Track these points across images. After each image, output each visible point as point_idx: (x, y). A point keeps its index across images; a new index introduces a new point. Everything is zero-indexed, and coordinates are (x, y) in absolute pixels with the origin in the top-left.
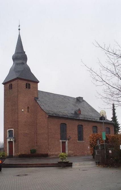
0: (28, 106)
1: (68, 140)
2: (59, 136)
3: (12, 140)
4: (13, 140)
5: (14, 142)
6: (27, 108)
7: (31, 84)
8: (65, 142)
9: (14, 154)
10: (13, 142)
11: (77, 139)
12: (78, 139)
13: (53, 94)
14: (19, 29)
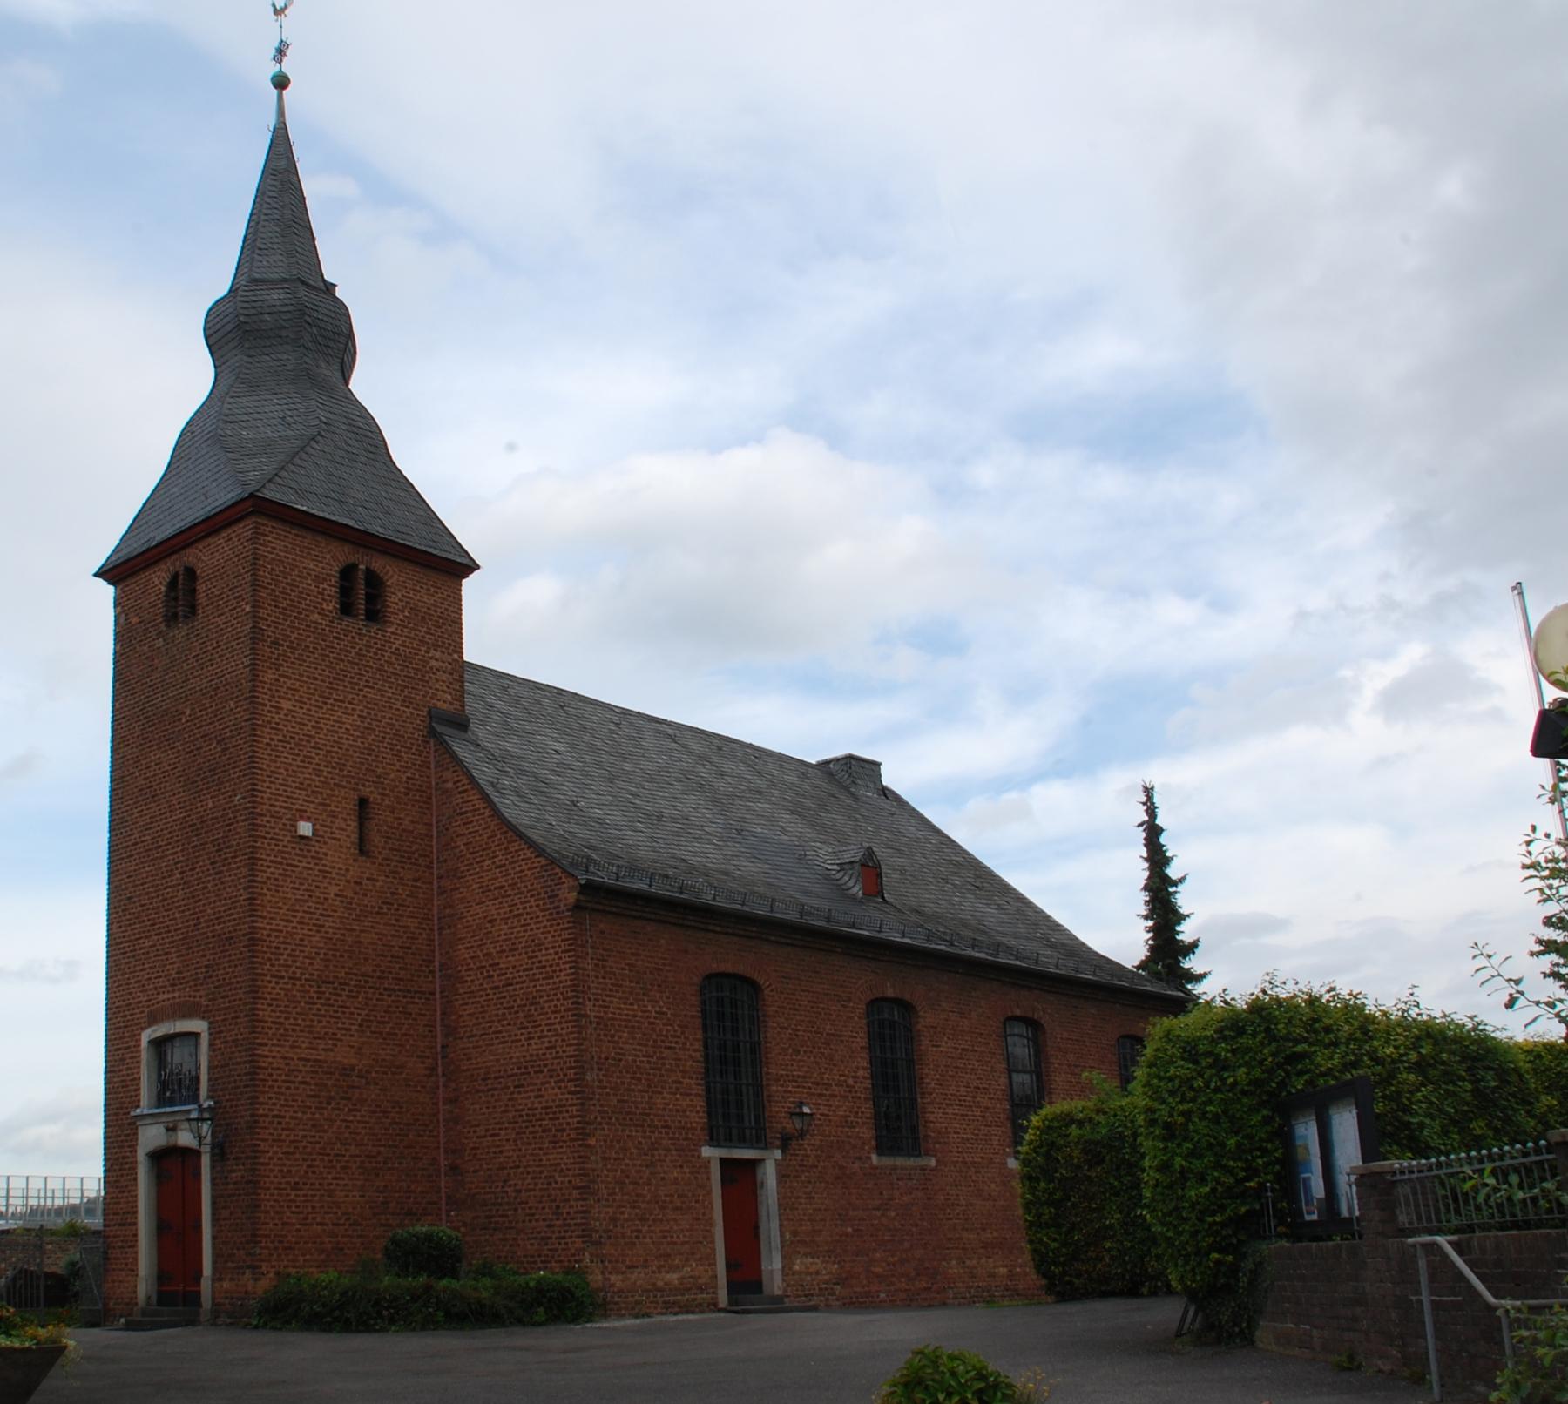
0: (366, 791)
1: (784, 1148)
2: (695, 1110)
3: (185, 1138)
4: (200, 1138)
5: (206, 1161)
6: (351, 806)
7: (395, 576)
8: (753, 1164)
9: (206, 1286)
10: (197, 1154)
11: (867, 1133)
12: (878, 1138)
13: (609, 707)
14: (281, 83)
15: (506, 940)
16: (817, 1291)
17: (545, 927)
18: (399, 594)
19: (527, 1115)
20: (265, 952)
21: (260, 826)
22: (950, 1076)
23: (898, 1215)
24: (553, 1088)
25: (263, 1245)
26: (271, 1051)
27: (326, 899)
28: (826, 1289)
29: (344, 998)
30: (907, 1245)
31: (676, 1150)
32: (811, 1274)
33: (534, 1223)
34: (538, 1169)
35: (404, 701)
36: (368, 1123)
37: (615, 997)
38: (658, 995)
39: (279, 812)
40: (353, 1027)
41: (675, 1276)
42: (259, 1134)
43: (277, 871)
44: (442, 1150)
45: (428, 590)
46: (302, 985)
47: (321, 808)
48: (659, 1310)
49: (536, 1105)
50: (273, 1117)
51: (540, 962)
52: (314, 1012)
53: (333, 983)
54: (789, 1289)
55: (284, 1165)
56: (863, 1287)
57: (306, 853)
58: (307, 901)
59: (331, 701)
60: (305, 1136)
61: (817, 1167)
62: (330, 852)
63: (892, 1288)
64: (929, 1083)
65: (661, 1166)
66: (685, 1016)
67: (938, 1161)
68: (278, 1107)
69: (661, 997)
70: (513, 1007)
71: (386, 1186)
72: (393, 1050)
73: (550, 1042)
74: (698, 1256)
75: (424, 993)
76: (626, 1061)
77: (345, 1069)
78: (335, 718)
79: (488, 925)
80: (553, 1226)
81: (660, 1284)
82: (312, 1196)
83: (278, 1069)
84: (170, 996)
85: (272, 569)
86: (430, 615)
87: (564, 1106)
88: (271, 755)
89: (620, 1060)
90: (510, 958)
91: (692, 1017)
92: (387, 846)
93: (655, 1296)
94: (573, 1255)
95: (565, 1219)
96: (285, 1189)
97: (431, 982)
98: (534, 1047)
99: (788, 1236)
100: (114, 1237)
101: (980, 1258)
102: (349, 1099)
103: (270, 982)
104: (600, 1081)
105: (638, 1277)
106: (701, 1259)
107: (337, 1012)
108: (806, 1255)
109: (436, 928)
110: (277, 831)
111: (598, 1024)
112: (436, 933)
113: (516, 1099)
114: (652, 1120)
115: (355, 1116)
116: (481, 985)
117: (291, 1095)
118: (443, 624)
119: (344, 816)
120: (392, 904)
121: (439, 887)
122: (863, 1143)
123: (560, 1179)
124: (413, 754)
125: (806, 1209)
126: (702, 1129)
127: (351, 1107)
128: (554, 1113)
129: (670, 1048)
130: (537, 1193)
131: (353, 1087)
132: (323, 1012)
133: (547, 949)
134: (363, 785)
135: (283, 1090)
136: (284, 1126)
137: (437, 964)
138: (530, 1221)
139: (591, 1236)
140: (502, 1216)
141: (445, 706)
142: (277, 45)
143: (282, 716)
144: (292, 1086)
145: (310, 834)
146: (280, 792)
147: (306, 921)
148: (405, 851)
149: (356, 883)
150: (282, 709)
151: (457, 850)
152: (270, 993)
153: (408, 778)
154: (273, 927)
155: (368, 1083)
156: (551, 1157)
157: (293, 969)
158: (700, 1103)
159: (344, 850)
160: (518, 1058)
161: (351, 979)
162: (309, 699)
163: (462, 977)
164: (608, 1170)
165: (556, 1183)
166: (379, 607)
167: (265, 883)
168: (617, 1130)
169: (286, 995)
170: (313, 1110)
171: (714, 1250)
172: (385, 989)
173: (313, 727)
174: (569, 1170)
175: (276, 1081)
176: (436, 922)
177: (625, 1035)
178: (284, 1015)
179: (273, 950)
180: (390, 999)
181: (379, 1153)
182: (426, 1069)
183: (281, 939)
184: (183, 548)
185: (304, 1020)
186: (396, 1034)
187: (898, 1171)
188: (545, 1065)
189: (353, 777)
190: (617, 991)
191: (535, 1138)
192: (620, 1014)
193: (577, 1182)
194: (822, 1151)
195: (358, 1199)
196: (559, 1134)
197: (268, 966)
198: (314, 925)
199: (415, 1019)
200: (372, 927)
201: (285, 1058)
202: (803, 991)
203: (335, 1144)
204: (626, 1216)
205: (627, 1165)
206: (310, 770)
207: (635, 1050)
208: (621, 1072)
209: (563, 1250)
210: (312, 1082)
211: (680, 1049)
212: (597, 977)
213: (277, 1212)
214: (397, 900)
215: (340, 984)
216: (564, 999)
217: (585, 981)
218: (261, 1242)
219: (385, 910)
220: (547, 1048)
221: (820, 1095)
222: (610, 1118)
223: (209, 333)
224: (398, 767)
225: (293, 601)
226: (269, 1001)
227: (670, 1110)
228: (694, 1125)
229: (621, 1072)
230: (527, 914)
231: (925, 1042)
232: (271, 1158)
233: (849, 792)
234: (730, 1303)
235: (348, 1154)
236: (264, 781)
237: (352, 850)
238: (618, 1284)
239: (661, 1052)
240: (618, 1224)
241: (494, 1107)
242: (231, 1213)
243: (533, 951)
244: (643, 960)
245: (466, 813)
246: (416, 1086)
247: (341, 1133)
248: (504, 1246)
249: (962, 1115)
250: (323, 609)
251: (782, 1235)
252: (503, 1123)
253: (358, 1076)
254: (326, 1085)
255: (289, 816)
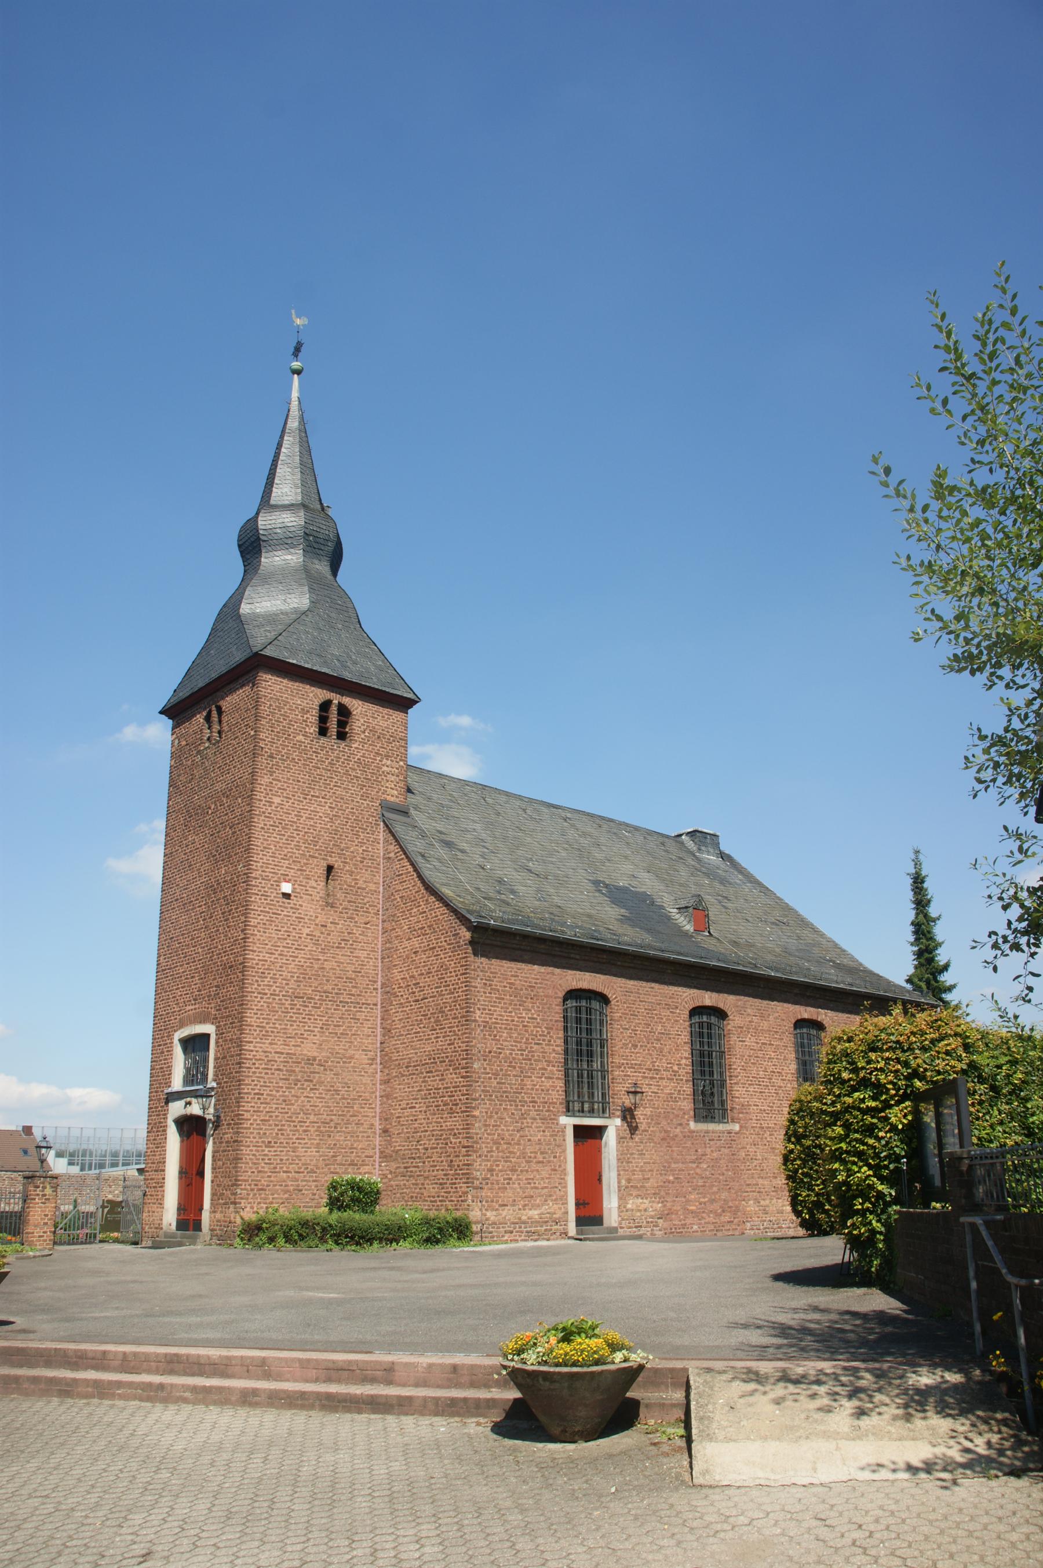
0: (331, 861)
2: (555, 1087)
6: (322, 871)
9: (206, 1217)
11: (687, 1105)
15: (424, 966)
16: (645, 1223)
17: (450, 957)
18: (362, 721)
19: (434, 1093)
20: (254, 976)
21: (254, 886)
22: (752, 1063)
23: (708, 1167)
24: (451, 1074)
25: (243, 1187)
26: (255, 1047)
27: (300, 938)
28: (652, 1222)
29: (310, 1008)
30: (715, 1189)
31: (541, 1119)
32: (640, 1211)
33: (435, 1172)
34: (440, 1133)
35: (362, 796)
36: (324, 1098)
37: (498, 1007)
38: (530, 1005)
39: (268, 876)
40: (316, 1029)
41: (536, 1212)
42: (244, 1106)
43: (265, 918)
44: (378, 1118)
45: (383, 717)
46: (279, 1000)
47: (299, 873)
48: (523, 1238)
49: (440, 1086)
50: (255, 1094)
51: (446, 982)
52: (288, 1018)
53: (302, 998)
54: (623, 1222)
55: (261, 1129)
56: (680, 1221)
57: (286, 905)
58: (286, 939)
59: (310, 797)
60: (277, 1108)
61: (647, 1131)
62: (304, 904)
63: (703, 1222)
64: (736, 1069)
65: (529, 1131)
66: (551, 1020)
67: (741, 1127)
68: (258, 1087)
69: (533, 1007)
70: (427, 1015)
71: (335, 1145)
72: (345, 1045)
73: (450, 1040)
74: (554, 1198)
75: (369, 1004)
76: (505, 1053)
77: (309, 1060)
78: (312, 809)
79: (413, 955)
80: (448, 1174)
81: (524, 1218)
82: (281, 1151)
83: (260, 1060)
84: (193, 1007)
85: (271, 705)
86: (383, 734)
87: (458, 1087)
88: (264, 836)
89: (500, 1053)
90: (427, 979)
91: (556, 1021)
92: (346, 899)
93: (520, 1227)
94: (461, 1197)
95: (456, 1170)
96: (261, 1147)
97: (375, 996)
98: (441, 1043)
99: (623, 1182)
100: (151, 1179)
101: (772, 1199)
102: (311, 1081)
103: (256, 997)
104: (485, 1069)
105: (507, 1213)
106: (556, 1200)
107: (304, 1018)
108: (637, 1196)
109: (380, 957)
110: (266, 889)
111: (485, 1027)
112: (380, 961)
113: (427, 1081)
114: (523, 1097)
115: (315, 1094)
116: (407, 998)
117: (269, 1078)
118: (394, 741)
119: (316, 878)
120: (348, 941)
121: (383, 928)
122: (684, 1113)
123: (453, 1141)
124: (368, 833)
125: (639, 1163)
126: (561, 1103)
127: (312, 1087)
128: (452, 1092)
129: (538, 1044)
130: (438, 1150)
131: (314, 1073)
132: (294, 1019)
133: (451, 972)
134: (331, 856)
135: (263, 1075)
136: (262, 1101)
137: (379, 983)
138: (433, 1171)
139: (473, 1183)
140: (415, 1167)
141: (392, 799)
142: (300, 354)
143: (273, 808)
144: (269, 1071)
145: (290, 892)
146: (270, 862)
147: (285, 953)
148: (360, 903)
149: (322, 926)
150: (273, 803)
151: (395, 902)
152: (256, 1005)
153: (363, 850)
154: (260, 958)
155: (325, 1070)
156: (448, 1124)
157: (274, 988)
158: (560, 1084)
159: (315, 903)
160: (429, 1051)
161: (316, 995)
162: (294, 796)
163: (395, 993)
164: (488, 1134)
165: (451, 1143)
166: (347, 730)
167: (256, 927)
168: (496, 1105)
169: (268, 1007)
170: (284, 1090)
171: (566, 1193)
172: (341, 1002)
173: (296, 815)
174: (459, 1133)
175: (258, 1068)
176: (380, 953)
177: (505, 1035)
178: (265, 1021)
179: (260, 974)
180: (344, 1009)
181: (332, 1120)
182: (369, 1059)
183: (266, 967)
184: (215, 692)
185: (280, 1024)
186: (347, 1034)
187: (710, 1134)
188: (447, 1057)
189: (323, 851)
190: (500, 1003)
191: (438, 1110)
192: (501, 1020)
193: (465, 1143)
194: (652, 1120)
195: (314, 1153)
196: (454, 1107)
197: (256, 986)
198: (291, 956)
199: (362, 1024)
200: (333, 957)
201: (265, 1052)
202: (641, 1001)
203: (299, 1114)
204: (500, 1168)
205: (503, 1130)
206: (292, 846)
207: (512, 1046)
208: (500, 1062)
209: (454, 1192)
210: (285, 1069)
211: (546, 1045)
212: (485, 993)
213: (255, 1164)
214: (352, 938)
215: (308, 998)
216: (461, 1009)
217: (476, 996)
218: (241, 1185)
219: (343, 945)
220: (449, 1045)
221: (652, 1078)
222: (491, 1096)
223: (241, 543)
224: (356, 843)
225: (285, 727)
226: (255, 1011)
227: (537, 1090)
228: (555, 1100)
229: (500, 1062)
230: (439, 947)
231: (734, 1038)
232: (251, 1124)
233: (694, 856)
234: (578, 1233)
235: (308, 1121)
236: (259, 854)
237: (321, 903)
238: (492, 1218)
239: (531, 1048)
240: (494, 1173)
241: (413, 1087)
242: (223, 1164)
243: (442, 974)
244: (520, 980)
245: (402, 874)
246: (360, 1072)
247: (304, 1106)
248: (415, 1189)
249: (761, 1092)
250: (306, 732)
251: (619, 1182)
252: (418, 1099)
253: (317, 1065)
254: (294, 1071)
255: (276, 879)
